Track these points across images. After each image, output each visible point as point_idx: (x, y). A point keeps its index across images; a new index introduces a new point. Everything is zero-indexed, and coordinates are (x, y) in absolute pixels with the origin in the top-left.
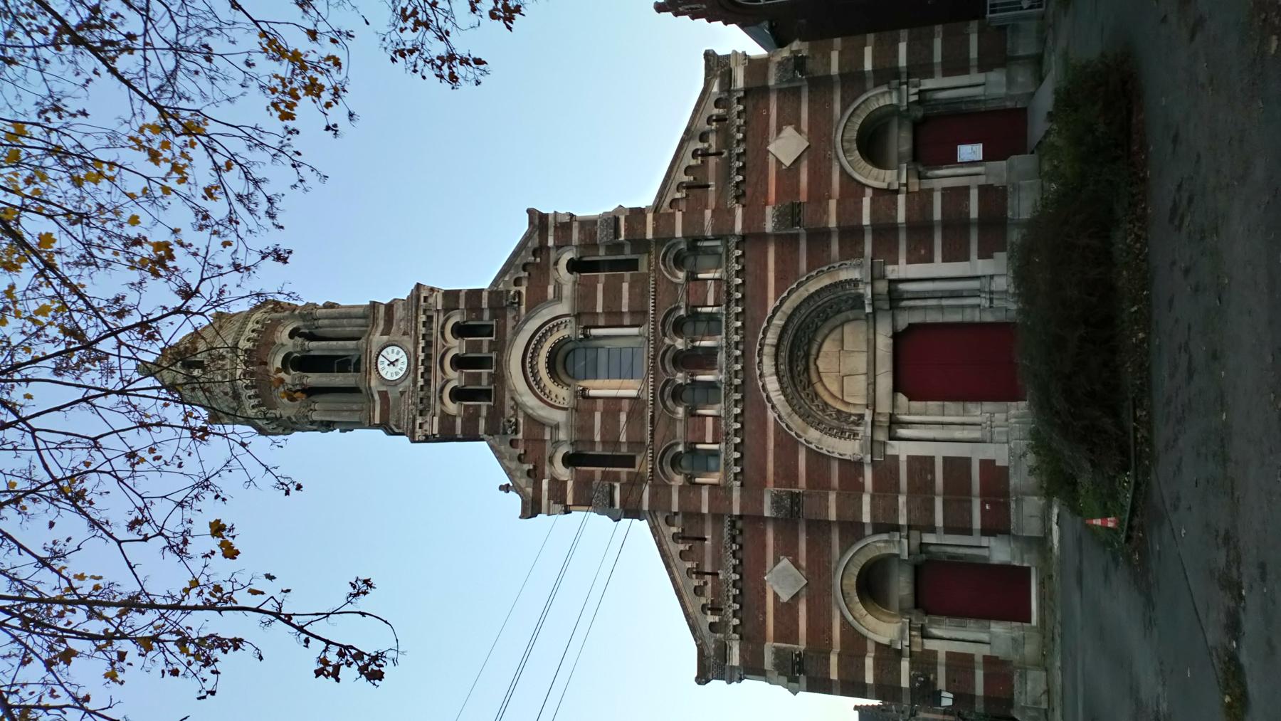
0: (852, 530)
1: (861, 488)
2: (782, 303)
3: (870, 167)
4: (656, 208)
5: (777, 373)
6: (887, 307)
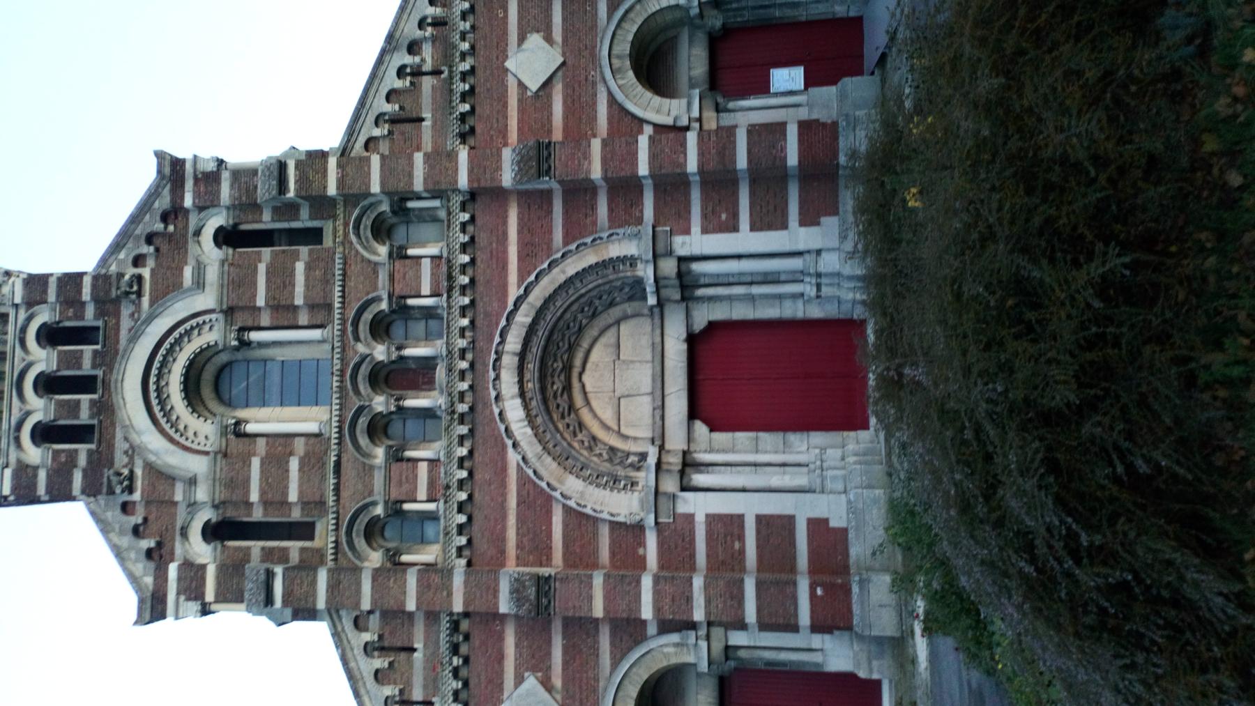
0: (629, 630)
1: (641, 564)
2: (527, 291)
3: (649, 94)
4: (344, 151)
5: (522, 394)
6: (678, 296)
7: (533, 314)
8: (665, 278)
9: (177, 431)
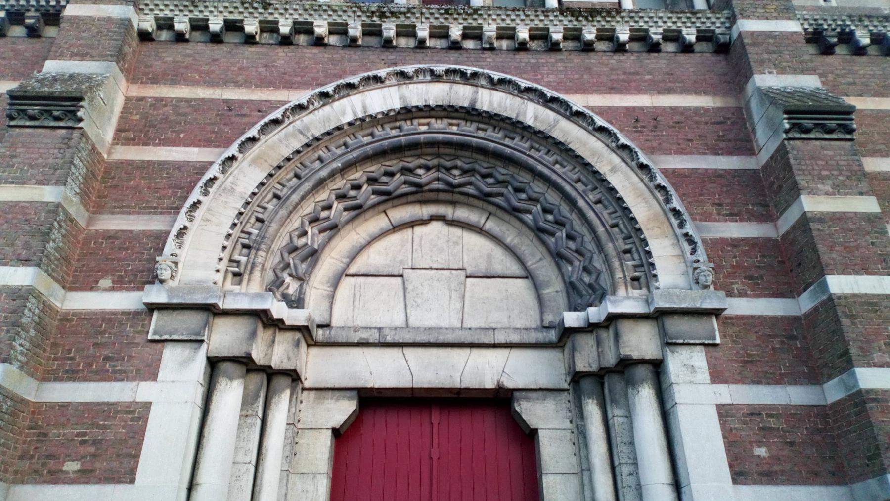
6: (581, 366)
7: (539, 126)
8: (617, 337)
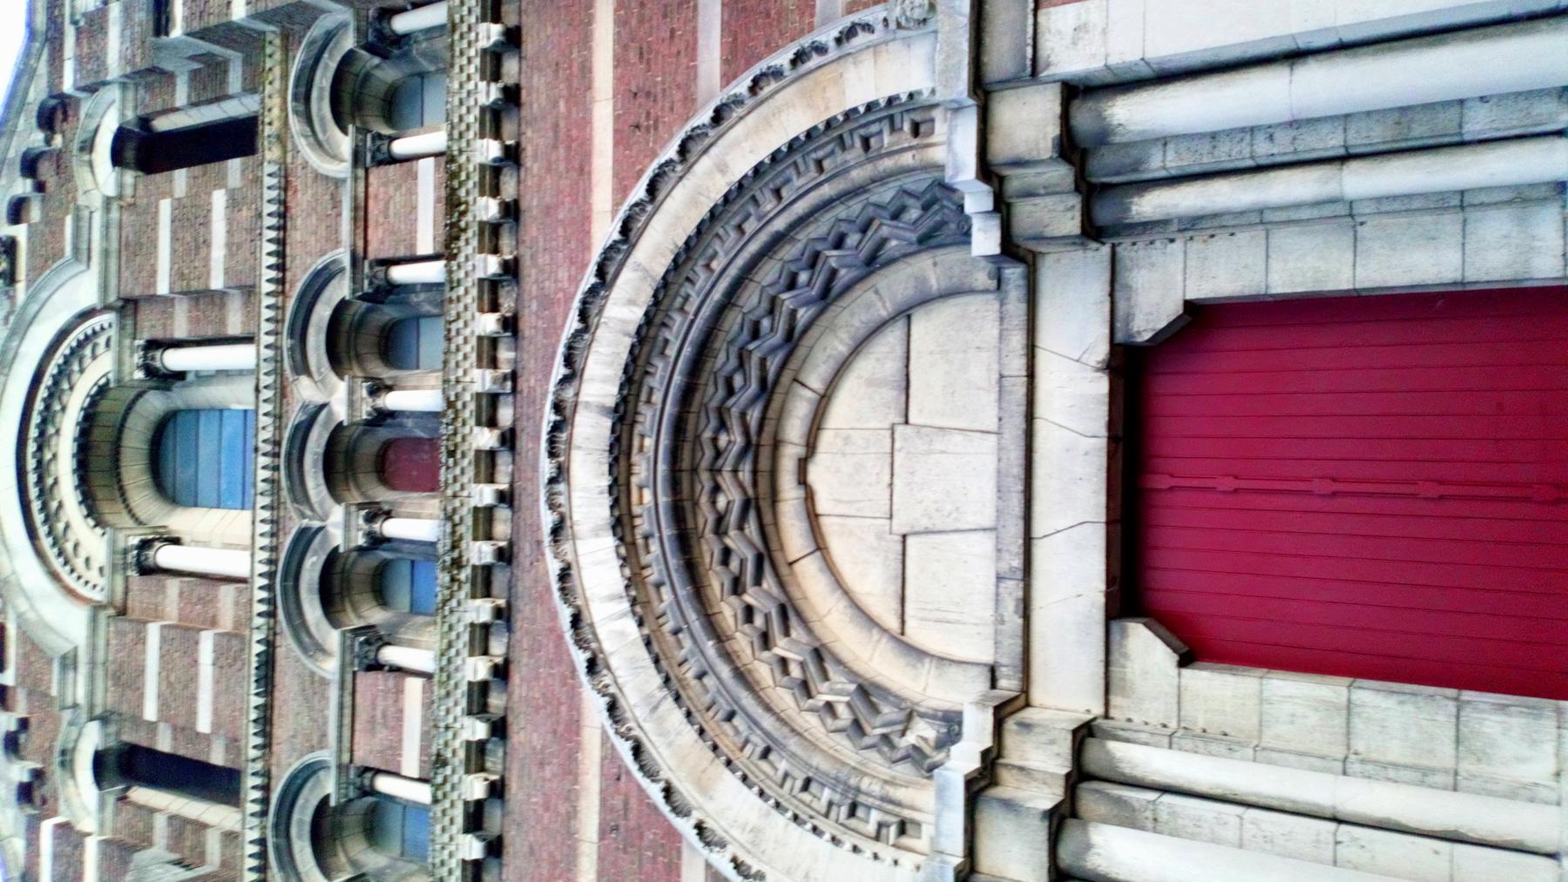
5: (621, 523)
6: (1071, 224)
8: (1018, 163)
9: (60, 554)
